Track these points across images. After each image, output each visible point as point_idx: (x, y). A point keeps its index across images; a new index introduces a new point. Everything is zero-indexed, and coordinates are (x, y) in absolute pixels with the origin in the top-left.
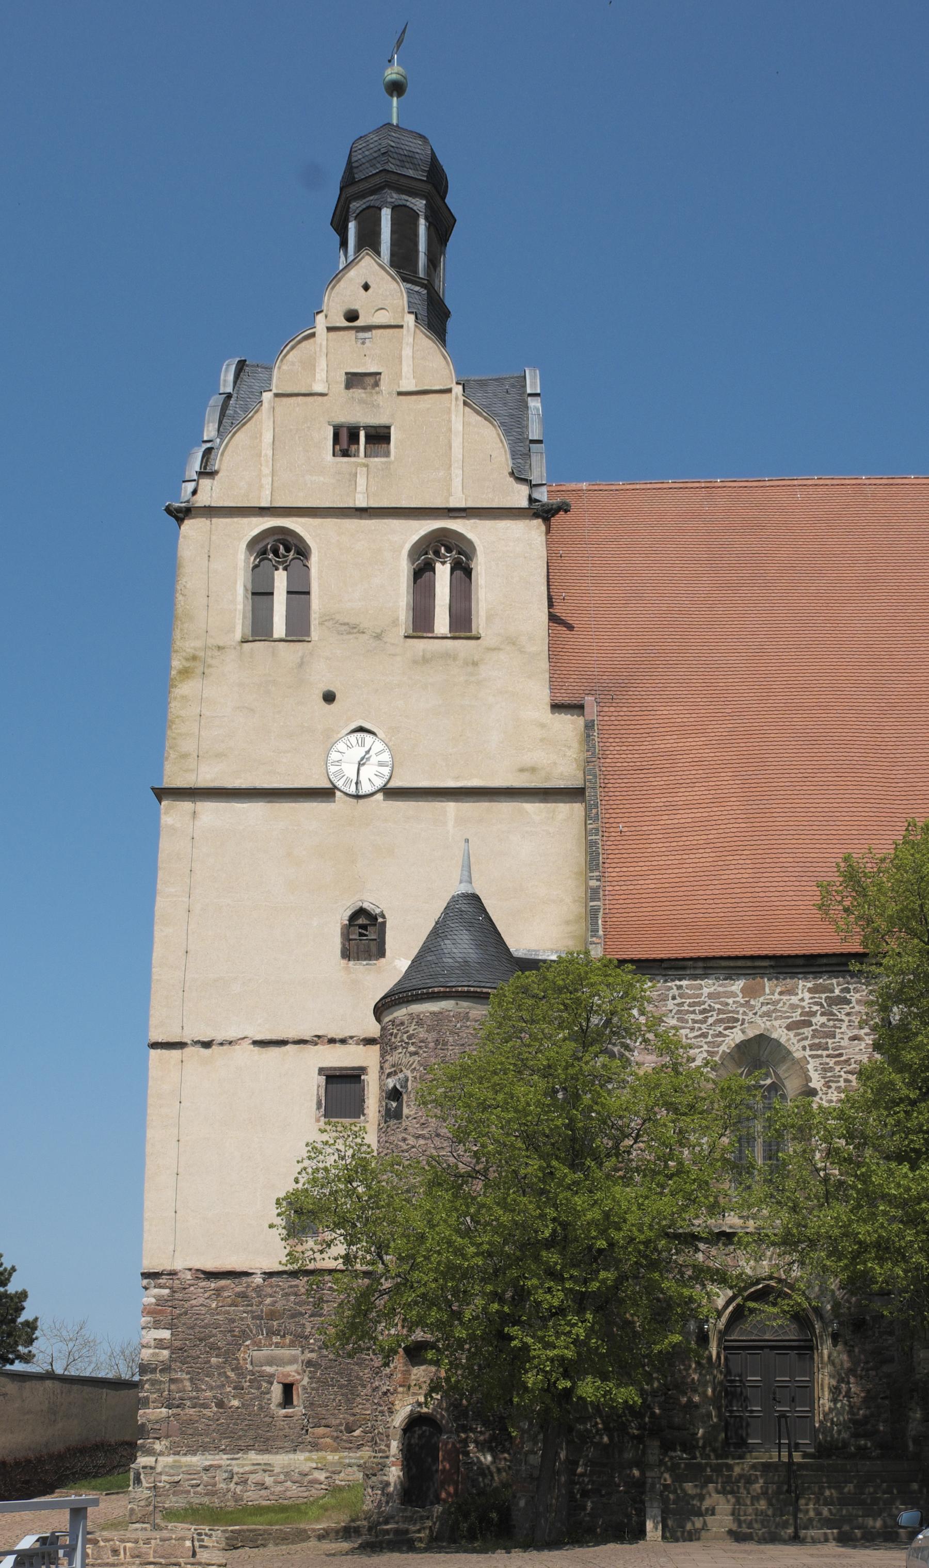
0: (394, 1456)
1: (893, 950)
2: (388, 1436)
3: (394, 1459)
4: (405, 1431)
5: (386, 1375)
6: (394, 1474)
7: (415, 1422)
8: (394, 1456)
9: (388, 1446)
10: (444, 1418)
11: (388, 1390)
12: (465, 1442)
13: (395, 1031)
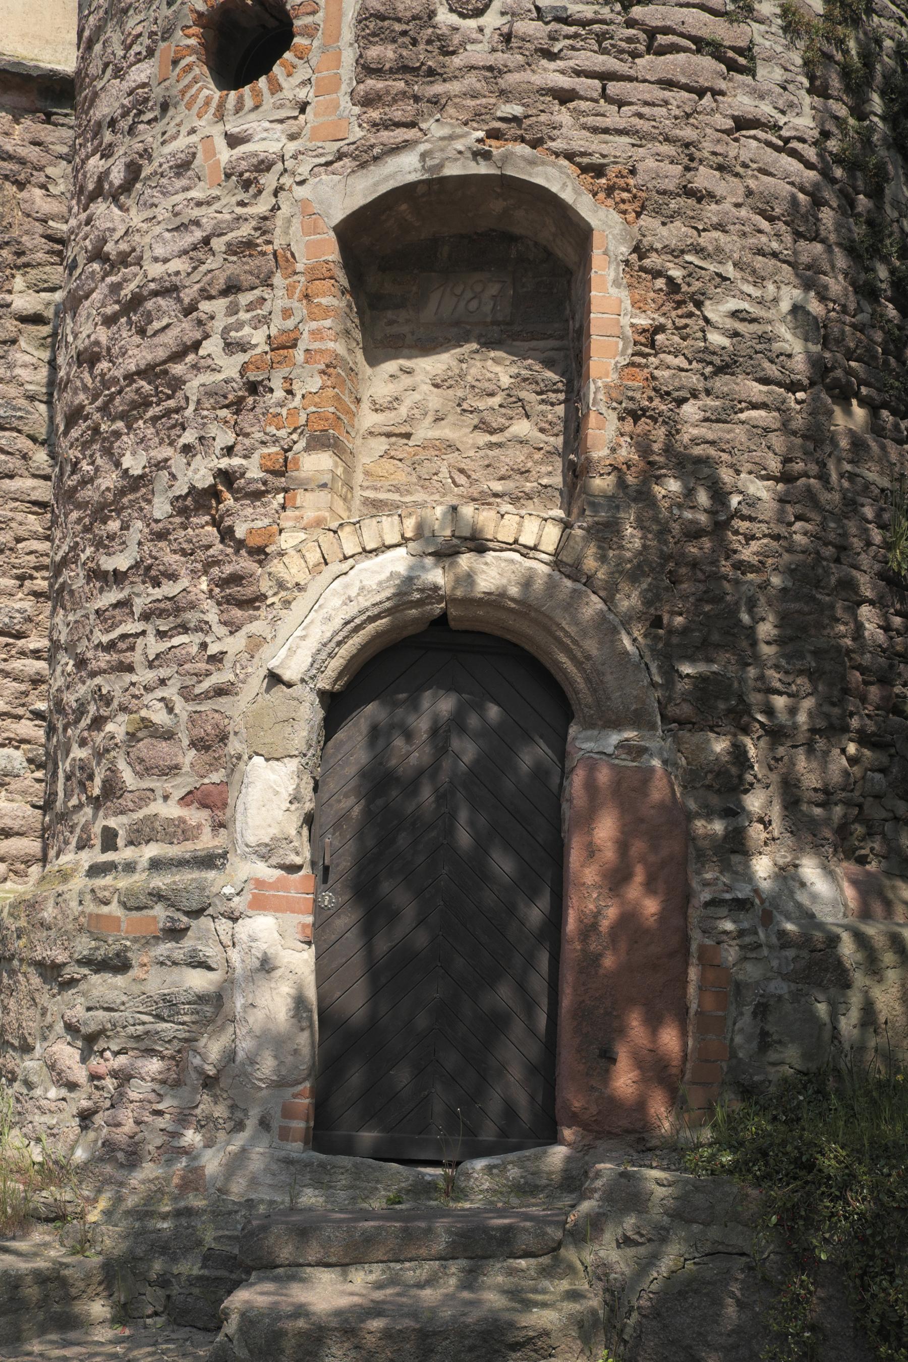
0: (265, 852)
1: (290, 290)
2: (210, 743)
3: (263, 870)
4: (336, 706)
5: (214, 395)
6: (274, 953)
7: (418, 651)
8: (265, 852)
9: (215, 802)
10: (603, 632)
11: (227, 477)
12: (725, 786)
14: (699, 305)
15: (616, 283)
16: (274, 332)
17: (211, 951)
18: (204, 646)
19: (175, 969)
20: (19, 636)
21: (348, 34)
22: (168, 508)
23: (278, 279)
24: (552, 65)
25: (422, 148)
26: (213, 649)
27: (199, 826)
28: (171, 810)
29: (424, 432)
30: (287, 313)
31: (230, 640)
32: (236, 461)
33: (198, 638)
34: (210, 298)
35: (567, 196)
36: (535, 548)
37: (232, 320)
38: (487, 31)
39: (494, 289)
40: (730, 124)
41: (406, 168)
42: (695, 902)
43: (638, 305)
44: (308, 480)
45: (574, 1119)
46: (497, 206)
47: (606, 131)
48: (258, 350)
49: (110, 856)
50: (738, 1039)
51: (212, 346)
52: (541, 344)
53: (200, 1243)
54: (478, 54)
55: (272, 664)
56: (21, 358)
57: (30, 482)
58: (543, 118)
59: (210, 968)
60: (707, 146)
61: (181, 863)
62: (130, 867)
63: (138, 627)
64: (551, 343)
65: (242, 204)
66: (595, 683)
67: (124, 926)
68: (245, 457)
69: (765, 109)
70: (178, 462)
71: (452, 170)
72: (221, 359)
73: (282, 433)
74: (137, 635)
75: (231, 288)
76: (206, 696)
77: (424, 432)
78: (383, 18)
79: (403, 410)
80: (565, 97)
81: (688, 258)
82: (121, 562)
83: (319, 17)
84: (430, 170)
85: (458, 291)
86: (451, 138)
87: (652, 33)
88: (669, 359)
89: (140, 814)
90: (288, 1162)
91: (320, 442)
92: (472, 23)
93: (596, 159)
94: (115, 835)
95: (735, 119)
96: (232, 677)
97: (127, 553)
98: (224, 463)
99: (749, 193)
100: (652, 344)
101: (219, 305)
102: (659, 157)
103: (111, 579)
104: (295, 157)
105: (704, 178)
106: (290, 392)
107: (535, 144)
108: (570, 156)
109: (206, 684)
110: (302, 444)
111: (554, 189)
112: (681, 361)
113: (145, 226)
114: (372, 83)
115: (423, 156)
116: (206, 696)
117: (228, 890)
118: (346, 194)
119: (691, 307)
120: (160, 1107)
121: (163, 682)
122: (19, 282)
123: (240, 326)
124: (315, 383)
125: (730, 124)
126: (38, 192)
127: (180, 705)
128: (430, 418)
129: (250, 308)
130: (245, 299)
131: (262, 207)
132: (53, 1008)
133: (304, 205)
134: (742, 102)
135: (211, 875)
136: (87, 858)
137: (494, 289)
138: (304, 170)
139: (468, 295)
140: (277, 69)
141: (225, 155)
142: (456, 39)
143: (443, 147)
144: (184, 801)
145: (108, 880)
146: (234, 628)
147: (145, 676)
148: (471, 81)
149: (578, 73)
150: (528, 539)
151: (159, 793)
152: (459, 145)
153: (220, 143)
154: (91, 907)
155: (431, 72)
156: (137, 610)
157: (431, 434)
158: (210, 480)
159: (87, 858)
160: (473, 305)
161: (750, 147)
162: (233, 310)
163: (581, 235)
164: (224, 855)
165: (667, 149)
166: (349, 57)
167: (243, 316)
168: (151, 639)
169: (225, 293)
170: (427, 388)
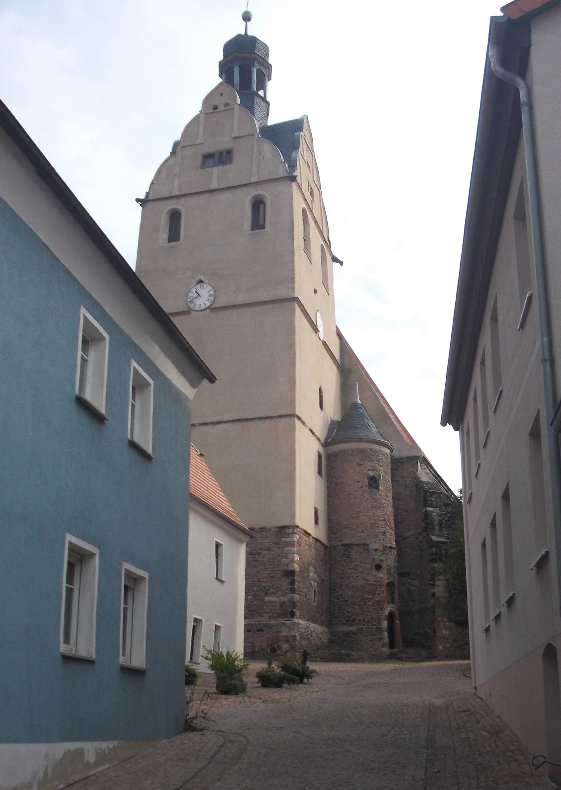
9: (380, 624)
13: (372, 454)
41: (390, 580)
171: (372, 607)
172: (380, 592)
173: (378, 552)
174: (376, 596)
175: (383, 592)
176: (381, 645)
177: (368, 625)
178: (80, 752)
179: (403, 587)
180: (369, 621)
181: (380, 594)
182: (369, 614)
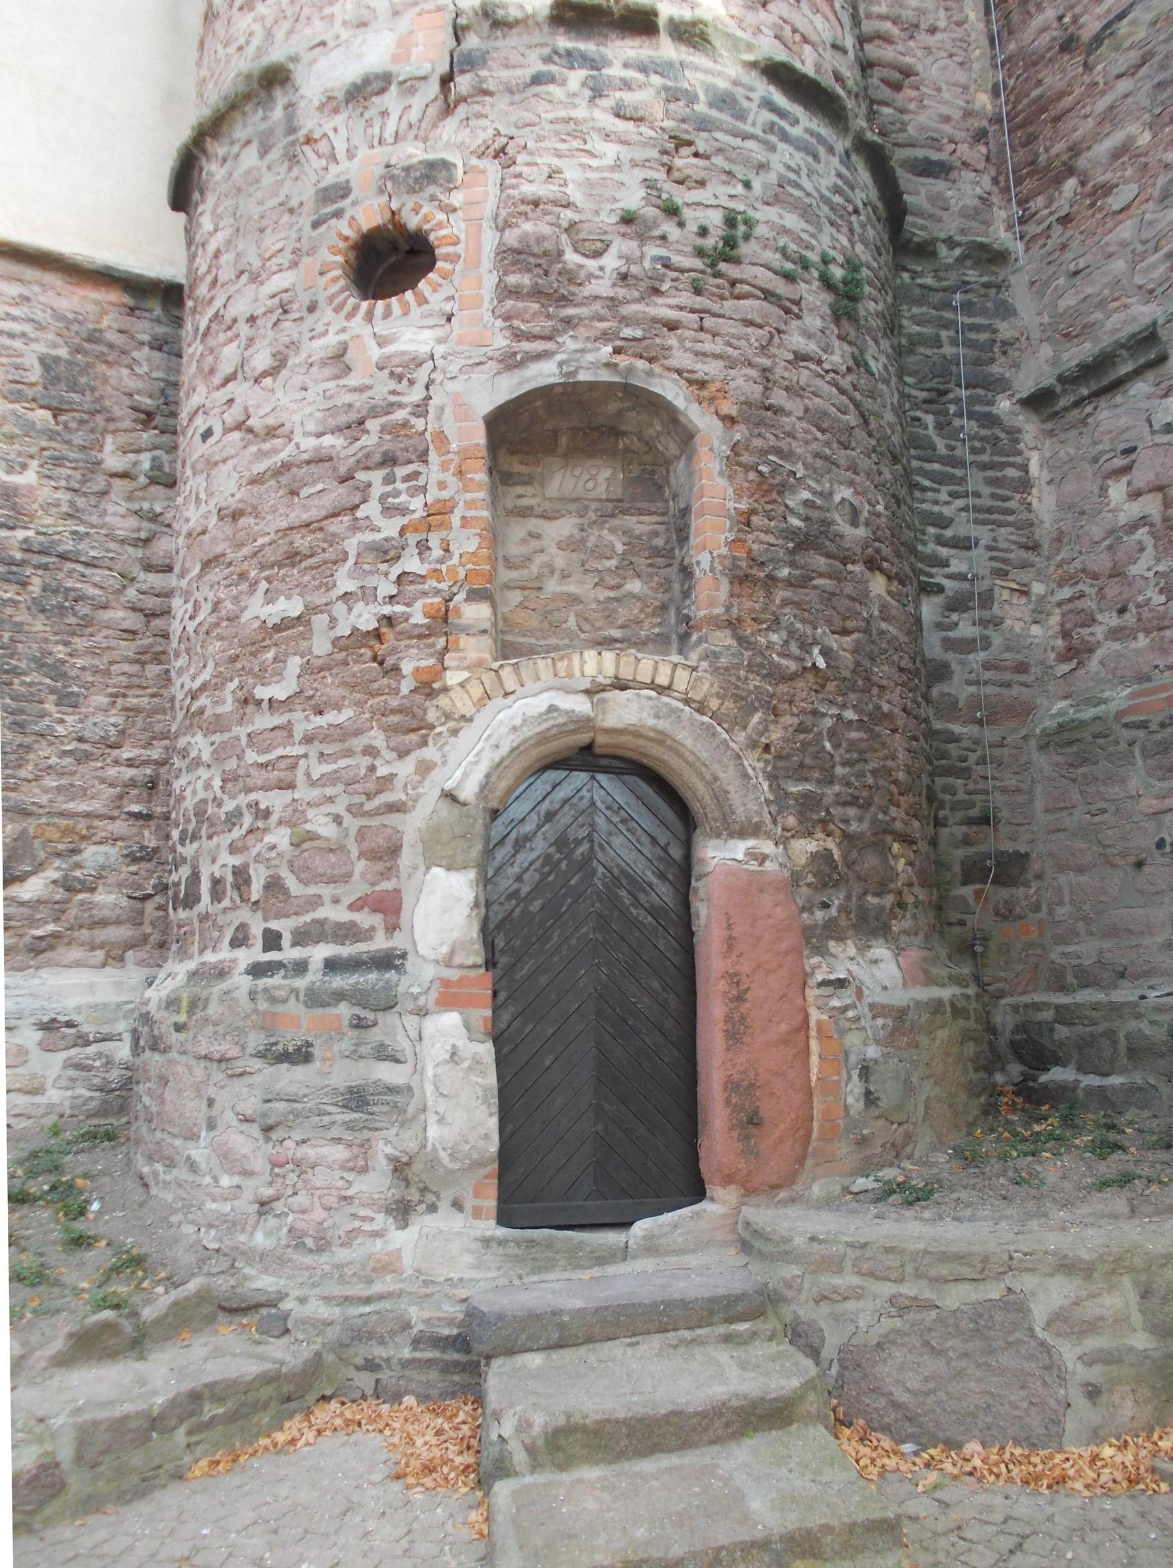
1: (444, 467)
9: (390, 908)
11: (389, 620)
14: (781, 493)
15: (721, 473)
16: (430, 501)
17: (402, 1043)
18: (372, 769)
19: (362, 1063)
20: (116, 746)
21: (487, 262)
22: (328, 648)
23: (433, 456)
24: (660, 300)
25: (560, 357)
26: (382, 771)
27: (373, 928)
28: (340, 914)
29: (552, 586)
30: (442, 485)
31: (399, 763)
32: (399, 609)
33: (367, 760)
34: (368, 468)
35: (680, 403)
36: (669, 688)
37: (389, 488)
38: (608, 270)
39: (606, 473)
40: (791, 357)
41: (545, 373)
42: (812, 982)
43: (739, 494)
44: (469, 627)
45: (729, 1180)
46: (613, 407)
47: (705, 354)
48: (417, 515)
49: (273, 956)
50: (850, 1100)
51: (371, 509)
52: (647, 519)
53: (407, 1326)
54: (603, 287)
55: (448, 785)
56: (111, 508)
57: (121, 614)
58: (658, 341)
59: (398, 1061)
60: (779, 371)
61: (354, 965)
62: (301, 967)
63: (298, 750)
64: (655, 518)
65: (393, 392)
66: (721, 797)
67: (305, 1023)
68: (408, 605)
69: (812, 347)
70: (339, 608)
71: (582, 377)
72: (379, 521)
73: (443, 586)
74: (299, 757)
75: (389, 460)
76: (377, 812)
77: (552, 586)
78: (520, 253)
79: (534, 569)
80: (672, 326)
81: (772, 458)
82: (280, 691)
83: (460, 249)
84: (568, 374)
85: (577, 472)
86: (583, 351)
87: (733, 283)
88: (763, 536)
89: (308, 918)
90: (486, 1242)
91: (475, 596)
92: (591, 264)
93: (699, 376)
94: (279, 936)
95: (795, 353)
96: (403, 797)
97: (284, 684)
98: (387, 610)
99: (807, 410)
100: (748, 524)
101: (376, 476)
102: (748, 379)
103: (265, 705)
104: (444, 357)
105: (778, 397)
106: (447, 550)
107: (651, 360)
108: (679, 372)
109: (377, 802)
110: (461, 596)
111: (670, 397)
112: (771, 539)
113: (294, 406)
114: (510, 303)
115: (561, 364)
116: (377, 812)
117: (415, 990)
118: (492, 391)
119: (774, 496)
120: (349, 1193)
121: (330, 800)
122: (109, 443)
123: (397, 494)
124: (472, 545)
125: (791, 357)
126: (125, 371)
127: (348, 820)
128: (557, 575)
129: (407, 478)
130: (401, 472)
131: (415, 395)
132: (222, 1098)
133: (457, 395)
134: (797, 341)
135: (392, 975)
136: (246, 957)
137: (606, 473)
138: (454, 369)
139: (585, 477)
140: (422, 285)
141: (375, 353)
142: (582, 274)
143: (580, 357)
144: (352, 907)
145: (276, 980)
146: (403, 754)
147: (304, 793)
148: (597, 307)
149: (681, 308)
150: (662, 680)
151: (326, 899)
152: (590, 357)
153: (371, 343)
154: (263, 1006)
155: (563, 298)
156: (298, 736)
157: (558, 589)
158: (375, 625)
159: (246, 957)
160: (590, 485)
161: (803, 376)
162: (389, 480)
163: (687, 438)
164: (404, 956)
165: (753, 373)
166: (490, 280)
167: (400, 485)
168: (313, 759)
169: (382, 464)
170: (553, 550)
171: (304, 722)
172: (390, 528)
173: (391, 100)
174: (345, 583)
175: (438, 514)
176: (376, 1183)
177: (272, 941)
178: (820, 1025)
179: (1117, 491)
180: (274, 886)
181: (386, 553)
182: (275, 801)
